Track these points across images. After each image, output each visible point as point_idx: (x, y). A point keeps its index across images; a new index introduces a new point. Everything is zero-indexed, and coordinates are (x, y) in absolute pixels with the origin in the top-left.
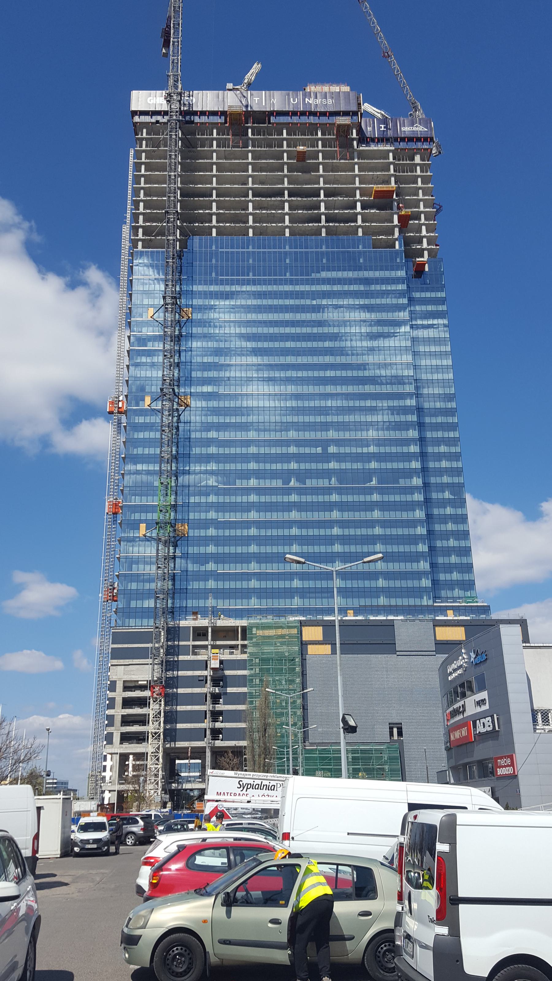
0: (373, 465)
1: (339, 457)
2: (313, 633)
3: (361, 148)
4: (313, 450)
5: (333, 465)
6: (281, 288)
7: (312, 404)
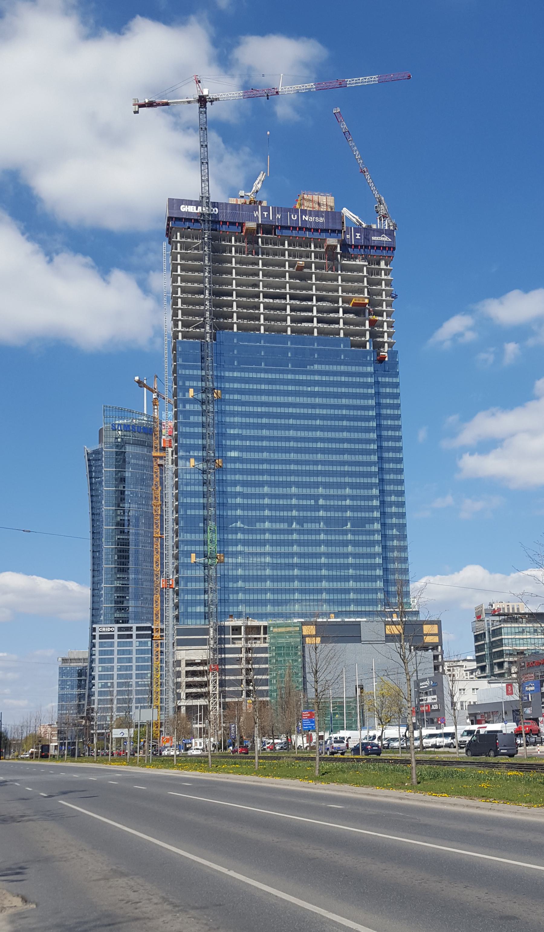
0: (349, 514)
1: (326, 508)
2: (308, 630)
3: (344, 262)
4: (308, 502)
5: (321, 513)
6: (285, 376)
7: (308, 468)
